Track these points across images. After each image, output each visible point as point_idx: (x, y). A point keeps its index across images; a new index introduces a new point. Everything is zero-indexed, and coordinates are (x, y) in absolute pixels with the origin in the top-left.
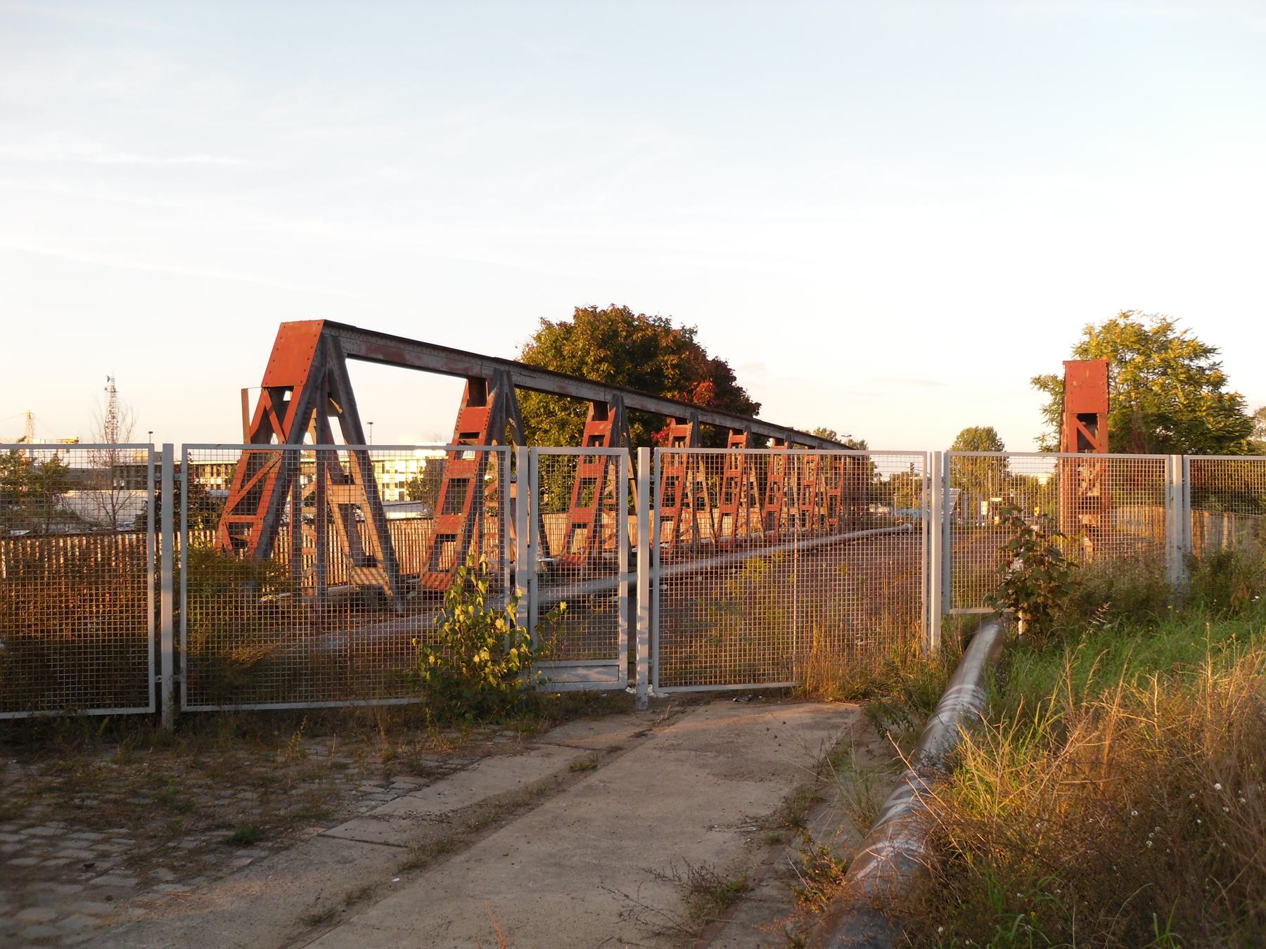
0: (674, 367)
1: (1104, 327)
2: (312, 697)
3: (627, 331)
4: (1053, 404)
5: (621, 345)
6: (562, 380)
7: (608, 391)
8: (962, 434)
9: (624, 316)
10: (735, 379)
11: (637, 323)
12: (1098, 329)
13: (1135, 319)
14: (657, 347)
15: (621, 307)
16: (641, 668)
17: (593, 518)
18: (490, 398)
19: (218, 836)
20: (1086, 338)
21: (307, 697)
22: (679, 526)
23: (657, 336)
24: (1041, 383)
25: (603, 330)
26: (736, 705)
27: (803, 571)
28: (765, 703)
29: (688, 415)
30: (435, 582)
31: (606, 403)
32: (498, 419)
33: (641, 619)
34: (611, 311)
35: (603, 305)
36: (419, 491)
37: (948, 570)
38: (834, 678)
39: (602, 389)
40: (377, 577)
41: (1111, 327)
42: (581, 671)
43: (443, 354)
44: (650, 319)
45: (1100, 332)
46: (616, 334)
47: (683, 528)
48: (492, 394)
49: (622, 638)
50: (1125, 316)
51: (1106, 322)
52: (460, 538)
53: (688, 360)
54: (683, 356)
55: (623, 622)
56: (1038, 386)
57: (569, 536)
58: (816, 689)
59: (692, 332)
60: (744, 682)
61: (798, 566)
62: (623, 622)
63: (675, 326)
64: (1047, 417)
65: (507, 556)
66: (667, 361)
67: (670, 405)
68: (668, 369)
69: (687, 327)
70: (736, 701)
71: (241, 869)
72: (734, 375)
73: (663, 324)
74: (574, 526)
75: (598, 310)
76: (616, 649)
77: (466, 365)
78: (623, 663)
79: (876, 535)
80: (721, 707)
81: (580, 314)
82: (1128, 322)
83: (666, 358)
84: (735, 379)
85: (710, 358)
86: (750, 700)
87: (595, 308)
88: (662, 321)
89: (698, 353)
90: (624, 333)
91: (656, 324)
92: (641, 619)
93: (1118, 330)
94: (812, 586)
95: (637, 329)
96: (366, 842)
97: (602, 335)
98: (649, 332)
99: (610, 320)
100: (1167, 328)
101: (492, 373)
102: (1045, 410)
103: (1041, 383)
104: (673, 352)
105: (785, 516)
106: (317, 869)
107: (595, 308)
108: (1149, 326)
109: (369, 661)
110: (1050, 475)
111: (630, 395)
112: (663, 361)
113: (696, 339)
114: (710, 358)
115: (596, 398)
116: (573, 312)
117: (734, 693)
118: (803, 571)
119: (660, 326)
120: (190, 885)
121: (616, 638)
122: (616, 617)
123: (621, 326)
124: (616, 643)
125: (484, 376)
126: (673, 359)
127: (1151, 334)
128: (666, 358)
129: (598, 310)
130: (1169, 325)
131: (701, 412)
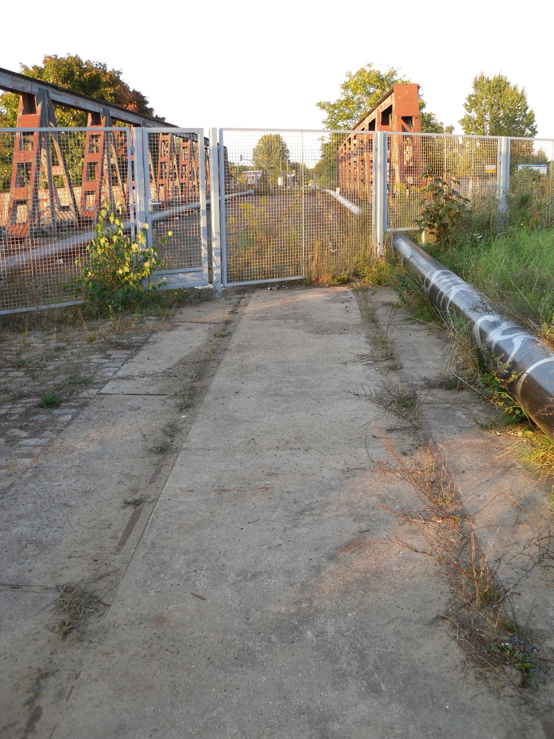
0: (111, 95)
1: (358, 73)
2: (15, 305)
3: (80, 72)
4: (328, 119)
5: (77, 81)
6: (76, 97)
7: (101, 105)
8: (262, 139)
9: (77, 62)
10: (147, 102)
11: (85, 66)
12: (354, 74)
13: (375, 68)
14: (99, 82)
15: (74, 56)
16: (217, 272)
17: (98, 187)
18: (39, 108)
19: (29, 403)
20: (347, 79)
21: (7, 306)
22: (100, 198)
23: (99, 75)
24: (322, 106)
25: (64, 70)
26: (271, 292)
27: (308, 203)
28: (287, 289)
29: (141, 123)
30: (17, 232)
31: (99, 114)
32: (44, 122)
33: (216, 239)
34: (68, 58)
35: (62, 54)
36: (476, 91)
37: (224, 226)
38: (328, 272)
39: (97, 104)
40: (70, 216)
41: (361, 73)
42: (181, 276)
43: (9, 76)
44: (94, 64)
45: (355, 75)
46: (72, 74)
47: (103, 198)
48: (40, 106)
49: (204, 252)
50: (369, 65)
51: (358, 69)
52: (30, 203)
53: (119, 91)
54: (117, 88)
55: (204, 241)
56: (320, 107)
57: (13, 211)
58: (317, 279)
59: (119, 73)
60: (276, 277)
61: (305, 200)
62: (204, 241)
63: (109, 69)
64: (325, 126)
65: (131, 202)
66: (107, 91)
67: (131, 115)
68: (107, 96)
69: (116, 70)
70: (271, 289)
71: (69, 423)
72: (147, 100)
73: (102, 67)
74: (85, 195)
75: (58, 58)
76: (200, 260)
77: (23, 85)
78: (206, 271)
79: (238, 197)
80: (265, 293)
81: (48, 60)
82: (372, 69)
83: (106, 89)
84: (147, 102)
85: (131, 90)
86: (278, 288)
87: (57, 56)
88: (101, 65)
89: (125, 88)
90: (78, 73)
91: (98, 67)
92: (216, 239)
93: (366, 75)
94: (313, 216)
95: (86, 70)
96: (140, 395)
97: (64, 74)
98: (94, 72)
99: (68, 64)
100: (393, 74)
101: (38, 91)
102: (324, 122)
103: (322, 106)
104: (110, 86)
105: (190, 186)
106: (122, 416)
107: (57, 56)
108: (384, 72)
109: (46, 278)
110: (318, 162)
111: (113, 109)
112: (104, 91)
113: (122, 78)
114: (131, 90)
115: (94, 110)
116: (43, 58)
117: (272, 284)
118: (308, 203)
119: (100, 68)
120: (44, 438)
121: (200, 253)
122: (200, 240)
123: (75, 68)
124: (200, 257)
125: (33, 93)
126: (110, 90)
127: (384, 77)
128: (106, 89)
129: (58, 58)
130: (395, 72)
131: (147, 120)
